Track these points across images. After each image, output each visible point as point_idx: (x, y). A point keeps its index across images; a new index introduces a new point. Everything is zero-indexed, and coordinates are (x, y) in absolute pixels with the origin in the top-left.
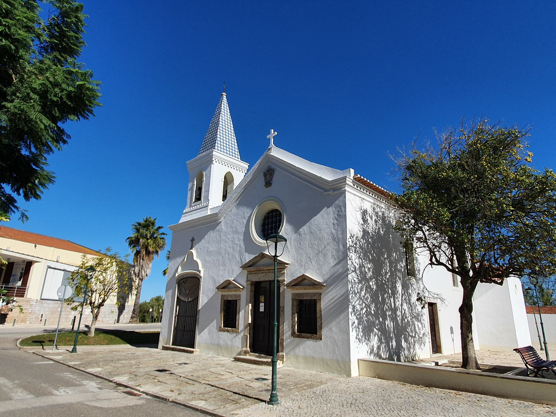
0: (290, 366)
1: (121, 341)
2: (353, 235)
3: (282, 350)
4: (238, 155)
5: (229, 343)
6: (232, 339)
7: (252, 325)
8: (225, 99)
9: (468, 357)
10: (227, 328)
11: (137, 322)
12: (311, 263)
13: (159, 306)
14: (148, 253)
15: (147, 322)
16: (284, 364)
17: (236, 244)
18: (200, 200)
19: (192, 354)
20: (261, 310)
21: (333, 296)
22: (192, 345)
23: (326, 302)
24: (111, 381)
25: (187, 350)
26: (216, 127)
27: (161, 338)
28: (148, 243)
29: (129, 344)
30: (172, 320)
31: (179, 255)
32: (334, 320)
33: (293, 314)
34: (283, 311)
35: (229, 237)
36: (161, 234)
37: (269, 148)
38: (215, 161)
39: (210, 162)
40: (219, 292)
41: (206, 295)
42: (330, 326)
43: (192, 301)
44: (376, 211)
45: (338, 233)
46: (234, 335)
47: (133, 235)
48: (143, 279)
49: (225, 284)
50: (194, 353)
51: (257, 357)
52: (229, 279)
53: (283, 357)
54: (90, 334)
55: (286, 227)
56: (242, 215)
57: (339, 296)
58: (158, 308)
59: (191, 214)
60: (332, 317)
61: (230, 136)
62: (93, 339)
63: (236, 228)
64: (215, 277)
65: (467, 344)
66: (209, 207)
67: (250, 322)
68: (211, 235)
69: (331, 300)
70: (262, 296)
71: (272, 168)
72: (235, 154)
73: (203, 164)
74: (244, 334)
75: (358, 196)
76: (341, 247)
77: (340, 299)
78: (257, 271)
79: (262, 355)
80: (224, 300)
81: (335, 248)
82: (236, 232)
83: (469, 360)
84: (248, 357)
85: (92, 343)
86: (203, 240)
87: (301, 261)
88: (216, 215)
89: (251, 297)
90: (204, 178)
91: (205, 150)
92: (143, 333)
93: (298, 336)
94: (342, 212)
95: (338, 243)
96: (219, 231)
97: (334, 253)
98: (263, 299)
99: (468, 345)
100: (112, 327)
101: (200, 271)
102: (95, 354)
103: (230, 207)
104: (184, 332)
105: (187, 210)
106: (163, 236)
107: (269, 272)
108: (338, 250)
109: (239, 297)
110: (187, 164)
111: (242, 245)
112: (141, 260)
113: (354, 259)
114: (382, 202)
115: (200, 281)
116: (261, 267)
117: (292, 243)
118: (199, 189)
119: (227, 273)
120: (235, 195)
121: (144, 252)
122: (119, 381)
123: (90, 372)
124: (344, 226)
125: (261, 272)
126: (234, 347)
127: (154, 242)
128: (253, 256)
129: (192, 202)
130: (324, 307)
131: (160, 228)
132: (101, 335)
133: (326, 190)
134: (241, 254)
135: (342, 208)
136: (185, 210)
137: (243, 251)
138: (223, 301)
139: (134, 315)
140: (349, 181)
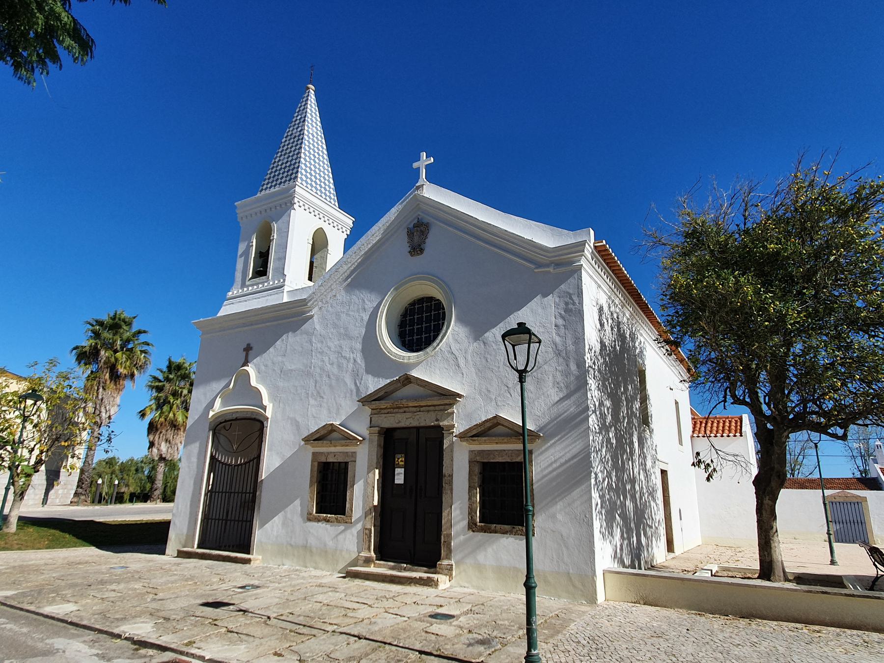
0: (466, 585)
1: (75, 540)
2: (591, 348)
3: (447, 555)
4: (335, 201)
5: (330, 544)
6: (337, 536)
7: (379, 509)
8: (313, 97)
9: (772, 561)
10: (325, 515)
11: (86, 503)
12: (509, 396)
13: (112, 474)
14: (115, 377)
15: (125, 502)
16: (453, 581)
17: (345, 358)
18: (266, 275)
19: (248, 565)
20: (397, 482)
21: (558, 455)
22: (246, 547)
23: (543, 467)
24: (119, 636)
25: (236, 558)
26: (297, 145)
27: (172, 534)
28: (116, 360)
29: (94, 546)
30: (200, 501)
31: (217, 378)
32: (559, 500)
33: (471, 488)
34: (451, 483)
35: (330, 344)
36: (143, 343)
37: (417, 185)
38: (297, 204)
39: (288, 204)
40: (309, 447)
41: (278, 453)
42: (553, 510)
43: (245, 463)
44: (611, 310)
45: (565, 342)
46: (342, 528)
47: (86, 343)
48: (101, 424)
49: (322, 433)
50: (252, 562)
51: (392, 568)
52: (331, 423)
53: (450, 568)
54: (7, 527)
55: (457, 329)
56: (358, 305)
57: (568, 456)
58: (111, 478)
59: (246, 301)
60: (556, 494)
61: (321, 164)
62: (16, 537)
63: (346, 329)
64: (297, 419)
65: (770, 539)
66: (286, 289)
67: (376, 503)
68: (290, 341)
69: (551, 464)
70: (400, 456)
71: (425, 221)
72: (330, 198)
73: (259, 214)
74: (364, 525)
75: (596, 282)
76: (573, 367)
77: (572, 462)
78: (394, 408)
79: (402, 565)
80: (319, 463)
81: (560, 368)
82: (348, 336)
83: (775, 566)
84: (372, 569)
85: (17, 547)
86: (271, 349)
87: (489, 391)
88: (303, 302)
89: (379, 456)
90: (275, 235)
91: (273, 184)
92: (113, 523)
93: (483, 530)
94: (574, 304)
95: (567, 361)
96: (307, 333)
97: (559, 378)
98: (402, 461)
99: (772, 542)
100: (39, 512)
101: (264, 408)
102: (37, 570)
103: (332, 290)
104: (226, 524)
105: (235, 292)
106: (145, 348)
107: (420, 411)
108: (566, 374)
109: (352, 456)
110: (235, 207)
111: (359, 361)
112: (101, 390)
113: (593, 389)
114: (618, 297)
115: (265, 425)
116: (404, 402)
117: (469, 358)
118: (263, 257)
119: (325, 412)
120: (346, 267)
121: (108, 374)
122: (138, 635)
123: (53, 615)
124: (580, 330)
125: (401, 410)
126: (341, 551)
127: (128, 358)
128: (383, 382)
129: (248, 279)
130: (539, 477)
131: (140, 332)
132: (31, 530)
133: (539, 265)
134: (356, 375)
135: (575, 298)
136: (230, 293)
137: (362, 370)
138: (316, 464)
139: (80, 490)
140: (588, 250)
